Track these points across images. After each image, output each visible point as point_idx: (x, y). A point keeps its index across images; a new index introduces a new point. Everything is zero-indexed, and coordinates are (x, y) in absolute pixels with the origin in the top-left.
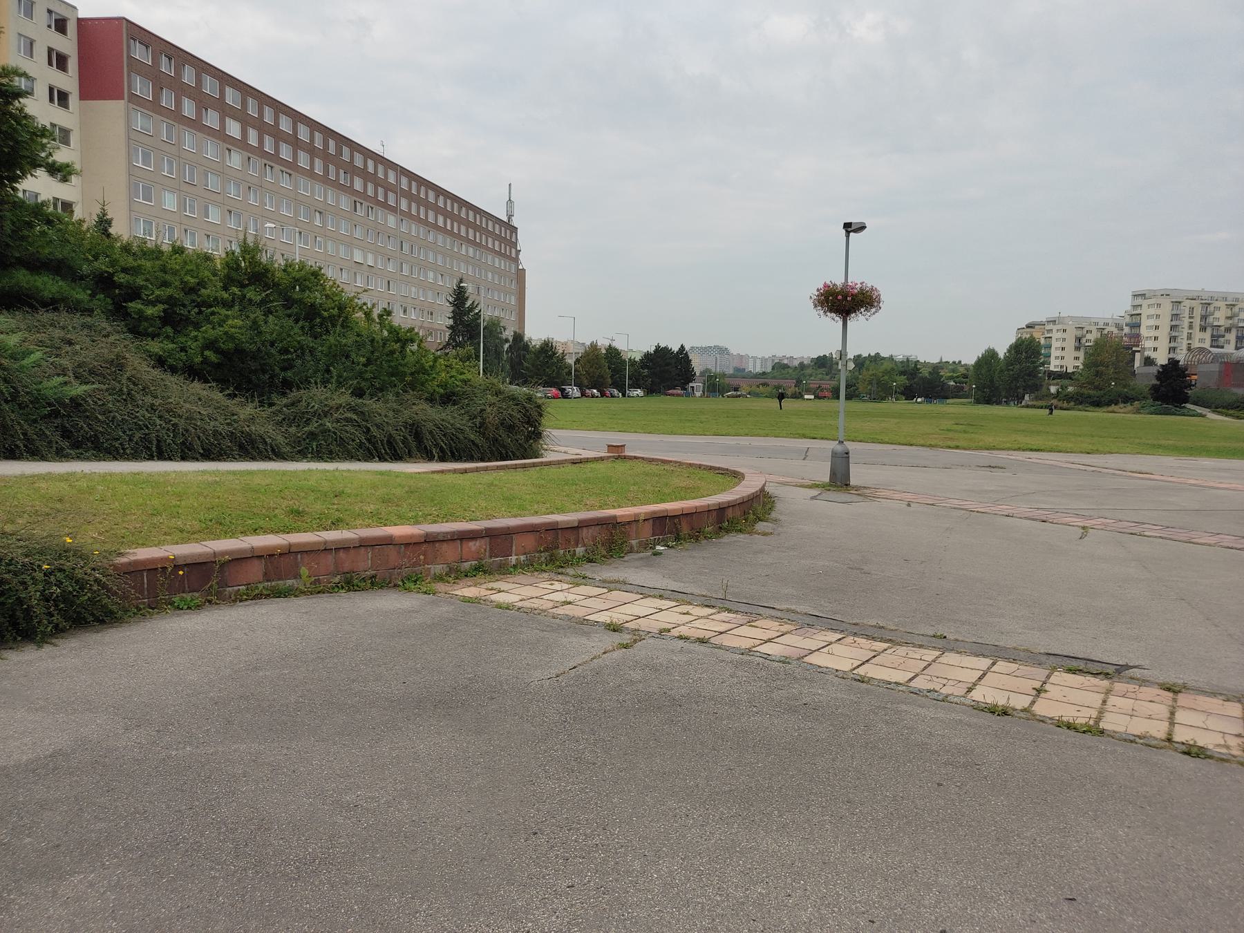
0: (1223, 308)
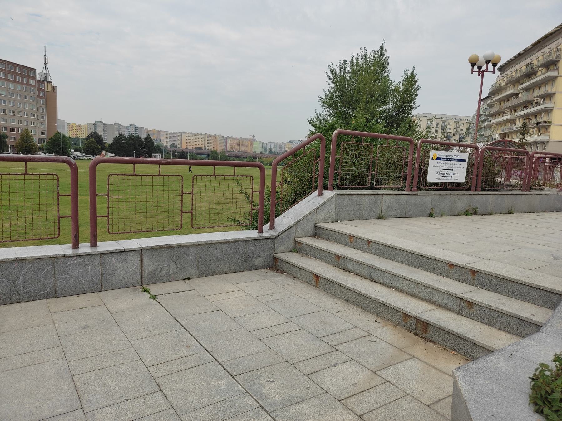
0: (453, 123)
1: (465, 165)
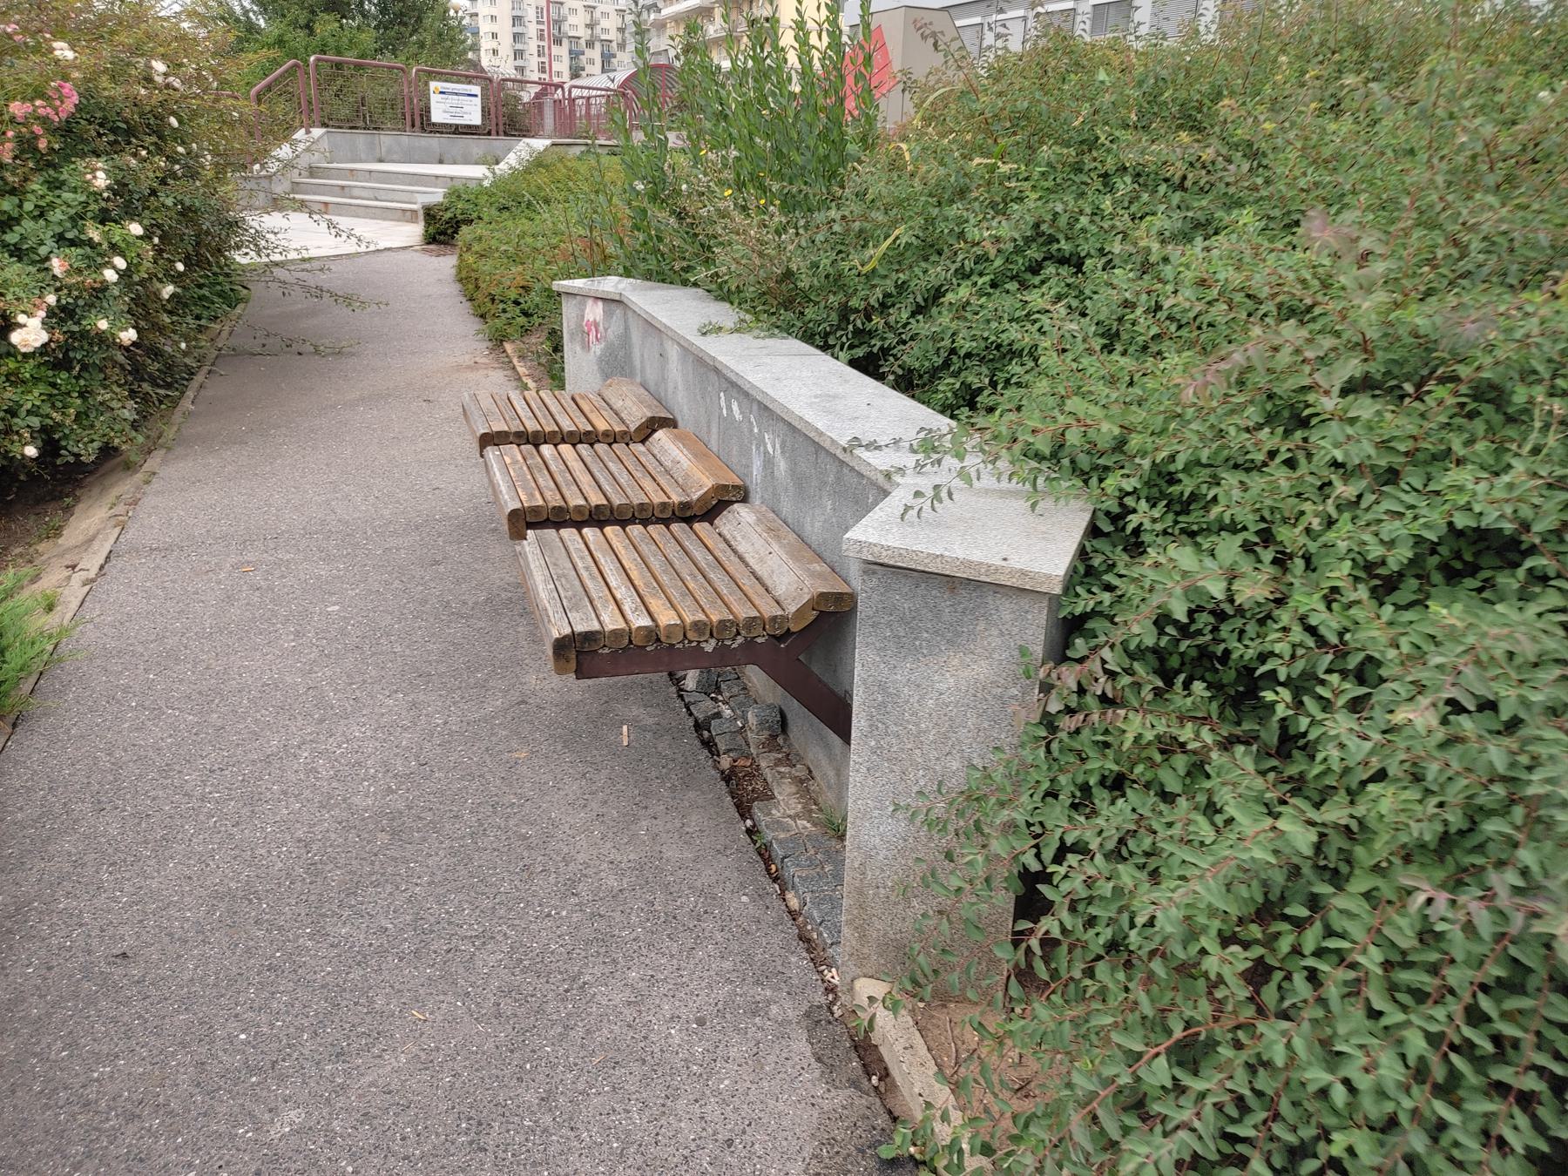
0: (613, 15)
1: (478, 101)
